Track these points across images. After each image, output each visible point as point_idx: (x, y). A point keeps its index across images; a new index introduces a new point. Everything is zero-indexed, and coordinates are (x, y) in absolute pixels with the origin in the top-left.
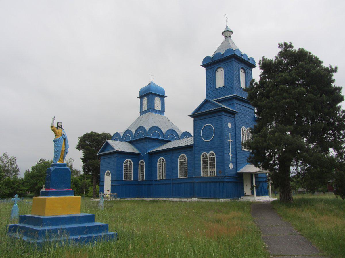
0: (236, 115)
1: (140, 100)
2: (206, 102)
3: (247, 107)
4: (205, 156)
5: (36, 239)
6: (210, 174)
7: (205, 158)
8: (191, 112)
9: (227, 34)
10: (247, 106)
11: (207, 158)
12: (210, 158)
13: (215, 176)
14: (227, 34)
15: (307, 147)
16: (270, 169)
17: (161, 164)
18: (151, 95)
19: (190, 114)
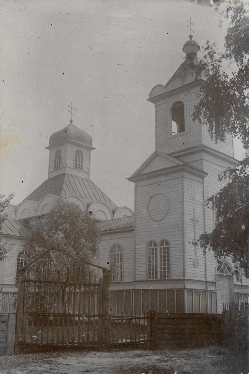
0: (205, 178)
1: (50, 152)
2: (156, 155)
3: (220, 166)
4: (164, 244)
5: (61, 325)
6: (161, 276)
7: (164, 248)
8: (131, 172)
9: (191, 37)
10: (220, 164)
11: (156, 249)
12: (161, 249)
13: (157, 279)
14: (191, 37)
15: (221, 237)
16: (22, 341)
17: (115, 255)
18: (67, 144)
19: (129, 177)
